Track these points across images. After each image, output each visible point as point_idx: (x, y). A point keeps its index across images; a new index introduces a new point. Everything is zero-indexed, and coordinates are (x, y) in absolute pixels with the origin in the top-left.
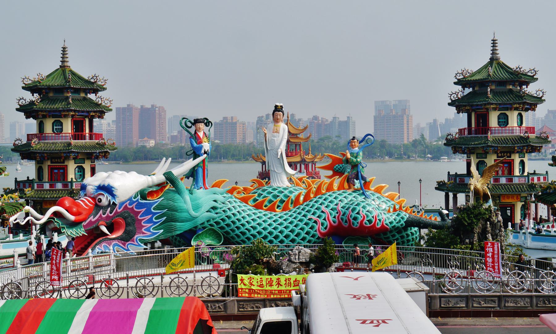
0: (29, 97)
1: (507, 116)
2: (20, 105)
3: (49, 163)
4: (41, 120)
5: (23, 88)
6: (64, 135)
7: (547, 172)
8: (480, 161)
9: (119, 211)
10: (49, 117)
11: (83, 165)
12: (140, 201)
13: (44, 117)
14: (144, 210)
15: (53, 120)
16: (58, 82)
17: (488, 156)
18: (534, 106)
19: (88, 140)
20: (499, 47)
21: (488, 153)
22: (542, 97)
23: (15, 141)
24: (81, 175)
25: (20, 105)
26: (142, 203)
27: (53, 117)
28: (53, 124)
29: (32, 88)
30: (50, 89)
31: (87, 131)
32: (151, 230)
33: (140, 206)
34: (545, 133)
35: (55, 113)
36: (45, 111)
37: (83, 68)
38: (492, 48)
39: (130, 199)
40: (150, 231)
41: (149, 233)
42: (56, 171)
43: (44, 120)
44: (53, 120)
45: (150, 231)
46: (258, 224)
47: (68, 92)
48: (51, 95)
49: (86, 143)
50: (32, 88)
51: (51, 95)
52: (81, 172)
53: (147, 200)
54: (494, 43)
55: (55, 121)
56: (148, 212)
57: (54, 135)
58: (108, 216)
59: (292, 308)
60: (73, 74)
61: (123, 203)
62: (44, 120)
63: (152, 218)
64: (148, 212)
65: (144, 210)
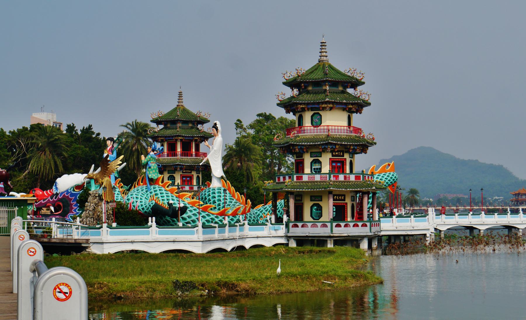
0: (289, 93)
2: (280, 100)
3: (330, 156)
4: (300, 113)
6: (322, 127)
8: (314, 160)
10: (308, 110)
11: (320, 203)
13: (303, 110)
15: (312, 113)
16: (318, 76)
17: (176, 172)
19: (179, 157)
20: (328, 48)
21: (177, 170)
22: (359, 97)
23: (109, 139)
25: (280, 100)
27: (312, 109)
29: (291, 84)
30: (307, 83)
31: (194, 150)
33: (72, 195)
35: (313, 106)
36: (163, 137)
37: (194, 107)
39: (67, 191)
42: (184, 179)
43: (303, 114)
44: (312, 113)
47: (326, 85)
48: (310, 88)
49: (164, 159)
50: (291, 84)
54: (180, 94)
57: (312, 128)
59: (381, 257)
60: (330, 67)
61: (62, 193)
62: (303, 114)
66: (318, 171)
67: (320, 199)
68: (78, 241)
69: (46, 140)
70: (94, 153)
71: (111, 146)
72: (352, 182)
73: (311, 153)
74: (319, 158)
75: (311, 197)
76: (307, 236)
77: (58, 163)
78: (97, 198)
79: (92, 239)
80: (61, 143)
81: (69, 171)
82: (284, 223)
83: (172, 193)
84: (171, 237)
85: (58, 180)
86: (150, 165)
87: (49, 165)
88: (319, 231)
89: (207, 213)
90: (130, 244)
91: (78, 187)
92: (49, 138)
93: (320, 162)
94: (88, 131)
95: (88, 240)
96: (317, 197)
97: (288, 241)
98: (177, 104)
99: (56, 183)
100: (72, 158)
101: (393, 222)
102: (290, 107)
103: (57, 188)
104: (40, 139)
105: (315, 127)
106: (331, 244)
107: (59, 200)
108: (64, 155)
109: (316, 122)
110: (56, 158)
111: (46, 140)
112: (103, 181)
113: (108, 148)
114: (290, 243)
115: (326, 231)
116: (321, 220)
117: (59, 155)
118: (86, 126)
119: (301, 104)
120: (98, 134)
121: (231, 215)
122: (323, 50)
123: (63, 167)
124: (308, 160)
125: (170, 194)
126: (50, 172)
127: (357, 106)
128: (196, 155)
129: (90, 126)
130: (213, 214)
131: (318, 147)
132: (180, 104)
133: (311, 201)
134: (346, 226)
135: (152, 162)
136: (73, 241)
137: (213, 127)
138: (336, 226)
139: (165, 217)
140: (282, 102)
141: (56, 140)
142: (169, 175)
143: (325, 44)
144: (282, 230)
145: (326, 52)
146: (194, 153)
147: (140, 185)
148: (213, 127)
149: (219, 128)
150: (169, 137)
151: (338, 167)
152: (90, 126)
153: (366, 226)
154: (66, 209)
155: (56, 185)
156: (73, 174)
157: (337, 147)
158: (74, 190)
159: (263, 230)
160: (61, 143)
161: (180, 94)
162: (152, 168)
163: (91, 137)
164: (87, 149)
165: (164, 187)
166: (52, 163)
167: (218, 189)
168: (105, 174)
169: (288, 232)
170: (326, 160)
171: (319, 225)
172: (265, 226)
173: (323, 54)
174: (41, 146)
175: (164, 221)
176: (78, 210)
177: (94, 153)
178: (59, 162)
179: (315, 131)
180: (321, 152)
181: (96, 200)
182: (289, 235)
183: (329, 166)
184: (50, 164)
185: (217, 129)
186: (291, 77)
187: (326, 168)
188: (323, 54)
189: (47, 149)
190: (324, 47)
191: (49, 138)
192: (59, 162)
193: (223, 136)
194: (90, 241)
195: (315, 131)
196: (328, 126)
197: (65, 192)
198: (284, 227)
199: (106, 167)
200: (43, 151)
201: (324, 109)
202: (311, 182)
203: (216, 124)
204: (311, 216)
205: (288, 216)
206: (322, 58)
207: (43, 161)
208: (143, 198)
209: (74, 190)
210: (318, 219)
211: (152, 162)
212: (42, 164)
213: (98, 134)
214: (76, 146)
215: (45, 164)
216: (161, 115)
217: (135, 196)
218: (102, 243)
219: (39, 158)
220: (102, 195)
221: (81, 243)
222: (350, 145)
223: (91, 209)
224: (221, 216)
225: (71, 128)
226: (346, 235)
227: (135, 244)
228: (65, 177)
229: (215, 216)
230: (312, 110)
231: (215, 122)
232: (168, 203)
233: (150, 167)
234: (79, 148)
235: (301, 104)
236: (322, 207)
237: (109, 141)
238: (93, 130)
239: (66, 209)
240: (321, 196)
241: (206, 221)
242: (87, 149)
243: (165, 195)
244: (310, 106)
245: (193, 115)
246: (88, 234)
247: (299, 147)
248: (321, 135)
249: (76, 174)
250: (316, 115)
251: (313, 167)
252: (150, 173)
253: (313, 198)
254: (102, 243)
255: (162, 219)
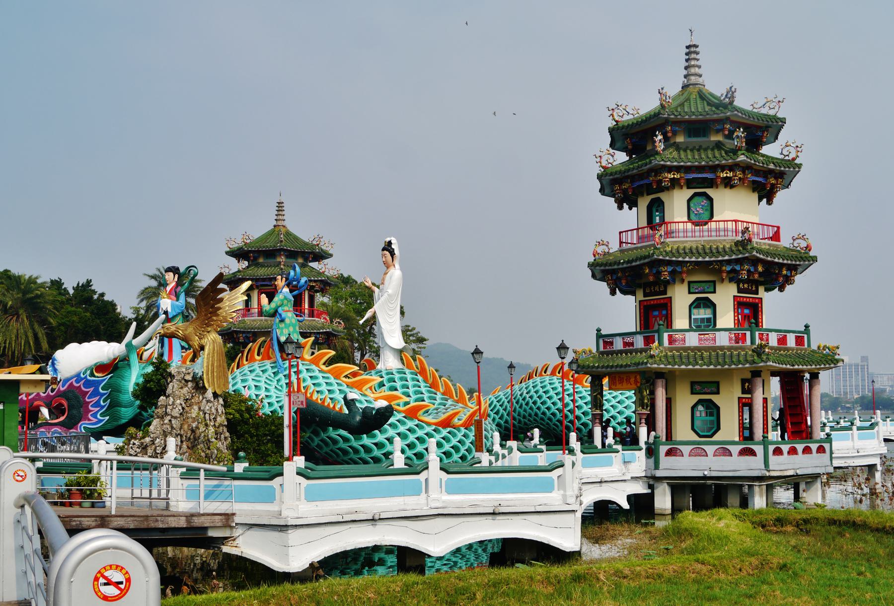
1: (711, 200)
2: (603, 167)
5: (227, 253)
7: (807, 327)
8: (697, 299)
9: (62, 389)
11: (714, 398)
12: (89, 378)
14: (92, 389)
15: (691, 192)
18: (776, 178)
20: (704, 58)
22: (794, 159)
23: (169, 270)
24: (712, 422)
25: (603, 167)
26: (90, 381)
27: (690, 184)
28: (689, 201)
29: (238, 254)
31: (307, 306)
32: (98, 416)
33: (88, 383)
34: (803, 238)
38: (685, 72)
39: (78, 375)
40: (96, 418)
41: (95, 420)
44: (691, 192)
45: (96, 418)
46: (376, 444)
49: (254, 321)
51: (261, 260)
52: (711, 414)
53: (94, 376)
54: (280, 206)
55: (695, 195)
56: (96, 393)
57: (689, 225)
58: (48, 395)
63: (99, 400)
64: (96, 393)
65: (92, 389)
66: (710, 324)
67: (716, 390)
68: (197, 522)
69: (20, 295)
70: (98, 321)
71: (174, 284)
72: (792, 349)
73: (690, 283)
74: (711, 296)
75: (693, 384)
76: (705, 478)
77: (40, 335)
78: (190, 384)
79: (244, 510)
80: (45, 302)
81: (83, 337)
82: (642, 444)
83: (337, 377)
84: (486, 500)
85: (59, 354)
86: (284, 315)
87: (24, 337)
88: (736, 465)
89: (417, 422)
90: (367, 528)
91: (101, 368)
92: (25, 293)
93: (712, 305)
94: (84, 290)
95: (228, 517)
96: (705, 386)
97: (651, 487)
98: (275, 223)
99: (54, 360)
100: (62, 328)
101: (853, 440)
102: (632, 182)
103: (55, 370)
104: (9, 295)
105: (696, 224)
106: (761, 496)
107: (60, 394)
108: (51, 323)
109: (701, 213)
110: (36, 326)
111: (20, 295)
112: (204, 342)
113: (169, 288)
114: (657, 492)
115: (754, 466)
116: (716, 438)
117: (43, 322)
118: (83, 281)
119: (670, 169)
120: (102, 295)
121: (462, 425)
122: (693, 63)
123: (49, 343)
124: (681, 298)
125: (332, 380)
126: (27, 350)
127: (768, 182)
128: (311, 315)
129: (89, 282)
130: (429, 424)
131: (708, 269)
132: (280, 223)
133: (692, 393)
134: (807, 450)
135: (286, 308)
136: (182, 523)
137: (383, 249)
138: (669, 453)
139: (325, 430)
140: (609, 171)
141: (37, 296)
142: (693, 297)
143: (697, 50)
144: (638, 463)
145: (699, 67)
146: (306, 311)
147: (256, 360)
148: (383, 249)
149: (397, 252)
150: (264, 280)
151: (749, 312)
152: (89, 282)
153: (752, 453)
154: (74, 412)
155: (53, 364)
156: (99, 340)
157: (760, 269)
158: (92, 375)
159: (609, 464)
160: (45, 302)
161: (280, 206)
162: (287, 321)
163: (92, 297)
164: (88, 314)
165: (317, 365)
166: (30, 334)
167: (388, 374)
168: (208, 325)
169: (657, 467)
170: (725, 297)
171: (710, 449)
172: (613, 455)
173: (693, 70)
174: (11, 307)
175: (323, 440)
176: (102, 415)
177: (98, 321)
178: (41, 333)
179: (697, 234)
180: (714, 282)
181: (185, 390)
182: (659, 474)
183: (732, 314)
184: (27, 336)
185: (392, 254)
186: (626, 118)
187: (726, 318)
188: (693, 70)
189: (21, 311)
190: (280, 217)
191: (25, 293)
192: (41, 333)
193: (401, 269)
194: (237, 519)
195: (706, 234)
196: (736, 221)
197: (72, 378)
198: (641, 454)
199: (213, 307)
200: (13, 316)
201: (728, 183)
202: (707, 349)
203: (390, 243)
204: (693, 429)
205: (651, 427)
206: (693, 78)
207: (15, 331)
208: (272, 388)
209: (92, 375)
210: (711, 436)
211: (286, 308)
212: (13, 336)
213: (102, 295)
214: (70, 309)
215: (17, 337)
216: (248, 241)
217: (252, 384)
218: (283, 528)
219: (8, 326)
220: (201, 378)
221: (205, 529)
222: (783, 265)
223: (176, 413)
224: (444, 427)
225: (57, 284)
226: (791, 473)
227: (381, 526)
228: (73, 347)
229: (434, 427)
230: (688, 188)
231: (388, 239)
232: (345, 398)
233: (282, 321)
234: (75, 313)
235: (670, 169)
236: (718, 408)
237: (171, 274)
238: (93, 288)
239: (74, 412)
240: (717, 384)
241: (418, 438)
242: (88, 314)
243: (321, 380)
244: (691, 176)
245: (306, 244)
246: (228, 497)
247: (670, 269)
248: (720, 241)
249: (95, 343)
250: (697, 200)
251: (693, 317)
252: (282, 333)
253: (697, 387)
254: (283, 528)
255: (317, 434)
